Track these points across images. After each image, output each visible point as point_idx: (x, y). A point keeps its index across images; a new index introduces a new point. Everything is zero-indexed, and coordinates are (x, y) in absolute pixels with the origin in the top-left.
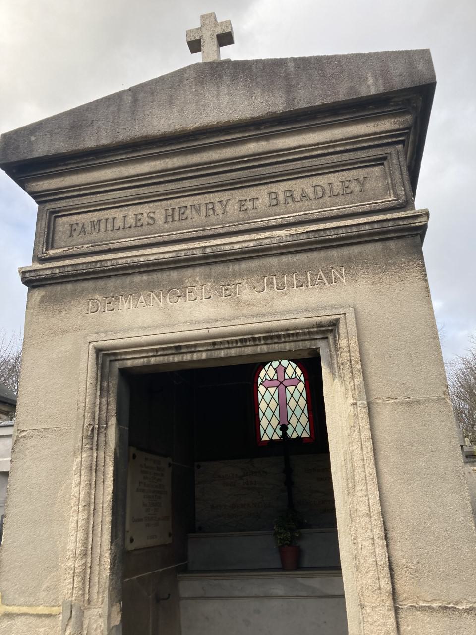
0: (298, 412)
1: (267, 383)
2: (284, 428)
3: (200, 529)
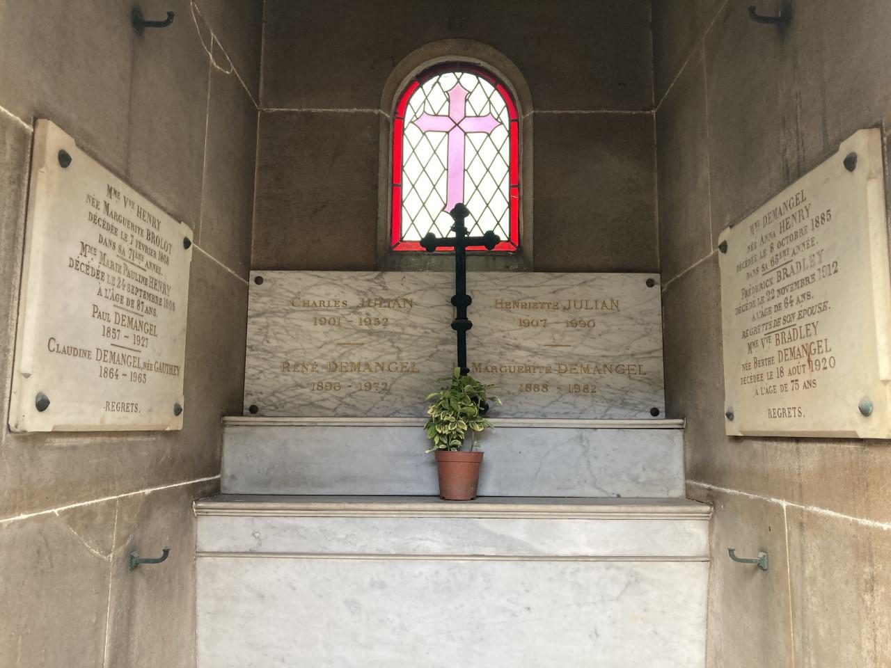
0: (488, 188)
1: (426, 122)
2: (460, 212)
3: (254, 410)
